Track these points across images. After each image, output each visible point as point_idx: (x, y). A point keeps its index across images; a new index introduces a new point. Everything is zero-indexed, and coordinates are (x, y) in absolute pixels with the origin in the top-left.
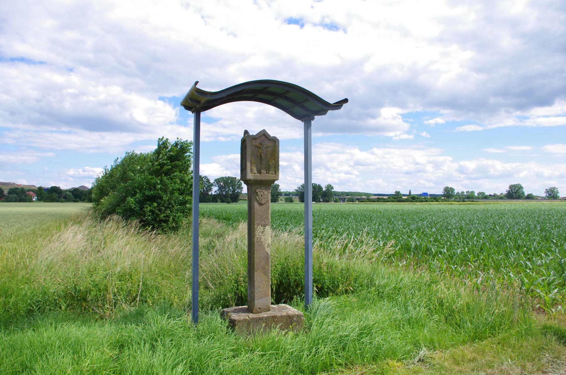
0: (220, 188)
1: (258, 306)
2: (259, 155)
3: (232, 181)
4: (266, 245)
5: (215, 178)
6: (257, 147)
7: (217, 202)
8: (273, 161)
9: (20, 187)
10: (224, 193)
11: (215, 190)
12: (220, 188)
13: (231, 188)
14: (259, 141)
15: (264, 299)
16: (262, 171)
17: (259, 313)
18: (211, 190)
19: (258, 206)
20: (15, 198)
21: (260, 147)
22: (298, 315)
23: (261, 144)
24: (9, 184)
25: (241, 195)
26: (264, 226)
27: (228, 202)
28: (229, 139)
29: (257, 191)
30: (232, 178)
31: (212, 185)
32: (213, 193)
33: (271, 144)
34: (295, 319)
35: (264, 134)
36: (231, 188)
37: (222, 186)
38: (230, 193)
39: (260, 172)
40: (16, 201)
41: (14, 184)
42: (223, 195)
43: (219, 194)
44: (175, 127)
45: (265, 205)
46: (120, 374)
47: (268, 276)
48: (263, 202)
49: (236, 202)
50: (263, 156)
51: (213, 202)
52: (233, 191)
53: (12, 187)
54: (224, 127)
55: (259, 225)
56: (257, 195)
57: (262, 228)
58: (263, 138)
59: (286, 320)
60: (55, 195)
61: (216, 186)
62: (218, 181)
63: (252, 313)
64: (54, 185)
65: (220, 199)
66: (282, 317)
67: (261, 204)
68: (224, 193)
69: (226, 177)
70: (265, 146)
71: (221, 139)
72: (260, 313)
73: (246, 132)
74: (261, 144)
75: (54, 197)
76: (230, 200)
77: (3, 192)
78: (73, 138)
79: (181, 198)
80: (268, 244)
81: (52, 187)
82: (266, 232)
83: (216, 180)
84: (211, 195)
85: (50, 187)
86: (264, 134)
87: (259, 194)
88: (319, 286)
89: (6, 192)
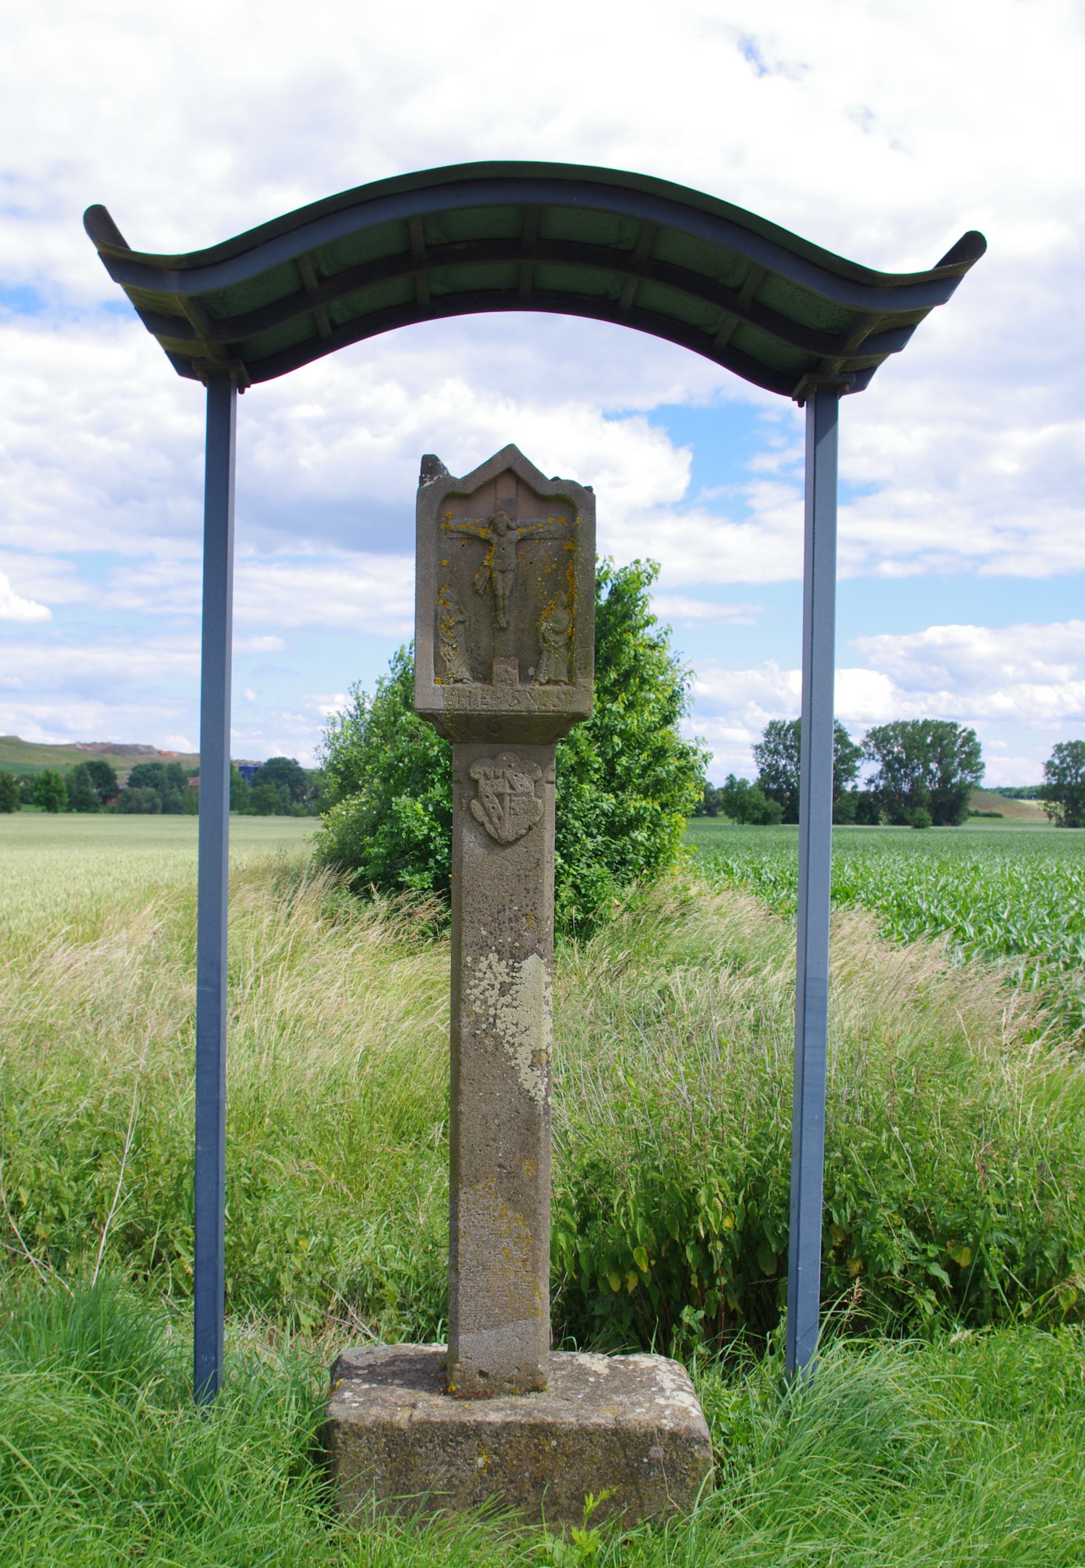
0: (888, 766)
1: (476, 1364)
2: (480, 584)
3: (938, 740)
4: (523, 1056)
5: (869, 727)
6: (473, 538)
7: (874, 821)
8: (563, 615)
9: (166, 761)
10: (906, 787)
11: (867, 774)
12: (890, 766)
13: (933, 766)
14: (483, 507)
15: (507, 1330)
16: (498, 668)
17: (478, 1396)
18: (850, 773)
19: (479, 851)
20: (150, 799)
21: (487, 542)
22: (674, 1436)
23: (492, 524)
24: (133, 750)
25: (973, 794)
26: (516, 955)
27: (919, 825)
28: (915, 569)
29: (476, 772)
30: (940, 725)
31: (856, 753)
32: (862, 788)
33: (550, 522)
34: (657, 1451)
35: (510, 472)
36: (933, 766)
37: (897, 759)
38: (931, 786)
39: (484, 674)
40: (152, 811)
41: (149, 749)
42: (901, 794)
43: (885, 792)
44: (695, 525)
45: (519, 848)
46: (33, 1566)
47: (531, 1214)
48: (508, 832)
49: (954, 823)
50: (503, 585)
51: (858, 820)
52: (945, 780)
53: (143, 760)
54: (899, 515)
55: (483, 948)
56: (477, 796)
57: (501, 968)
58: (506, 490)
59: (609, 1450)
60: (273, 791)
61: (871, 756)
62: (880, 737)
63: (445, 1393)
64: (278, 754)
65: (891, 810)
66: (584, 1433)
67: (495, 843)
68: (906, 787)
69: (914, 724)
70: (515, 535)
71: (888, 568)
72: (486, 1396)
73: (430, 465)
74: (492, 524)
75: (274, 797)
76: (927, 816)
77: (115, 777)
78: (334, 580)
79: (608, 802)
80: (536, 1053)
81: (273, 762)
82: (524, 991)
83: (873, 735)
84: (854, 794)
85: (264, 759)
86: (510, 472)
87: (485, 787)
88: (964, 1259)
89: (122, 779)
